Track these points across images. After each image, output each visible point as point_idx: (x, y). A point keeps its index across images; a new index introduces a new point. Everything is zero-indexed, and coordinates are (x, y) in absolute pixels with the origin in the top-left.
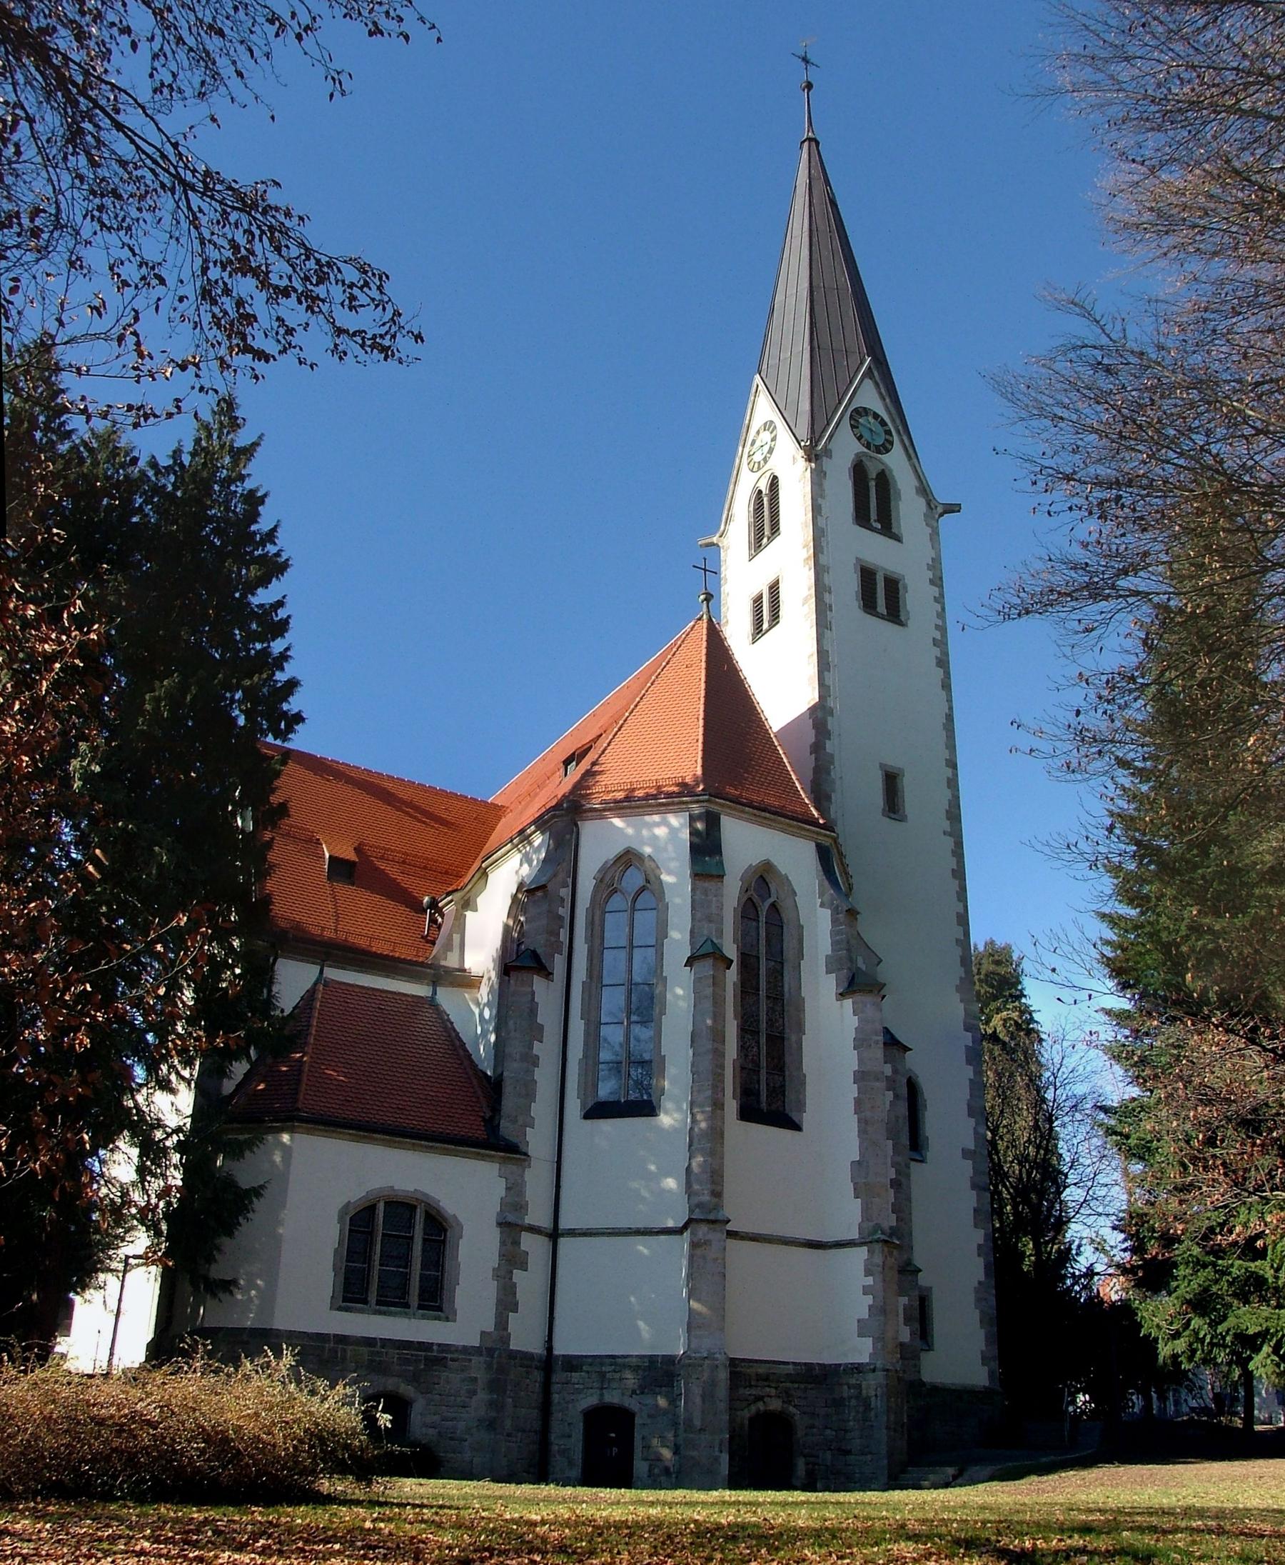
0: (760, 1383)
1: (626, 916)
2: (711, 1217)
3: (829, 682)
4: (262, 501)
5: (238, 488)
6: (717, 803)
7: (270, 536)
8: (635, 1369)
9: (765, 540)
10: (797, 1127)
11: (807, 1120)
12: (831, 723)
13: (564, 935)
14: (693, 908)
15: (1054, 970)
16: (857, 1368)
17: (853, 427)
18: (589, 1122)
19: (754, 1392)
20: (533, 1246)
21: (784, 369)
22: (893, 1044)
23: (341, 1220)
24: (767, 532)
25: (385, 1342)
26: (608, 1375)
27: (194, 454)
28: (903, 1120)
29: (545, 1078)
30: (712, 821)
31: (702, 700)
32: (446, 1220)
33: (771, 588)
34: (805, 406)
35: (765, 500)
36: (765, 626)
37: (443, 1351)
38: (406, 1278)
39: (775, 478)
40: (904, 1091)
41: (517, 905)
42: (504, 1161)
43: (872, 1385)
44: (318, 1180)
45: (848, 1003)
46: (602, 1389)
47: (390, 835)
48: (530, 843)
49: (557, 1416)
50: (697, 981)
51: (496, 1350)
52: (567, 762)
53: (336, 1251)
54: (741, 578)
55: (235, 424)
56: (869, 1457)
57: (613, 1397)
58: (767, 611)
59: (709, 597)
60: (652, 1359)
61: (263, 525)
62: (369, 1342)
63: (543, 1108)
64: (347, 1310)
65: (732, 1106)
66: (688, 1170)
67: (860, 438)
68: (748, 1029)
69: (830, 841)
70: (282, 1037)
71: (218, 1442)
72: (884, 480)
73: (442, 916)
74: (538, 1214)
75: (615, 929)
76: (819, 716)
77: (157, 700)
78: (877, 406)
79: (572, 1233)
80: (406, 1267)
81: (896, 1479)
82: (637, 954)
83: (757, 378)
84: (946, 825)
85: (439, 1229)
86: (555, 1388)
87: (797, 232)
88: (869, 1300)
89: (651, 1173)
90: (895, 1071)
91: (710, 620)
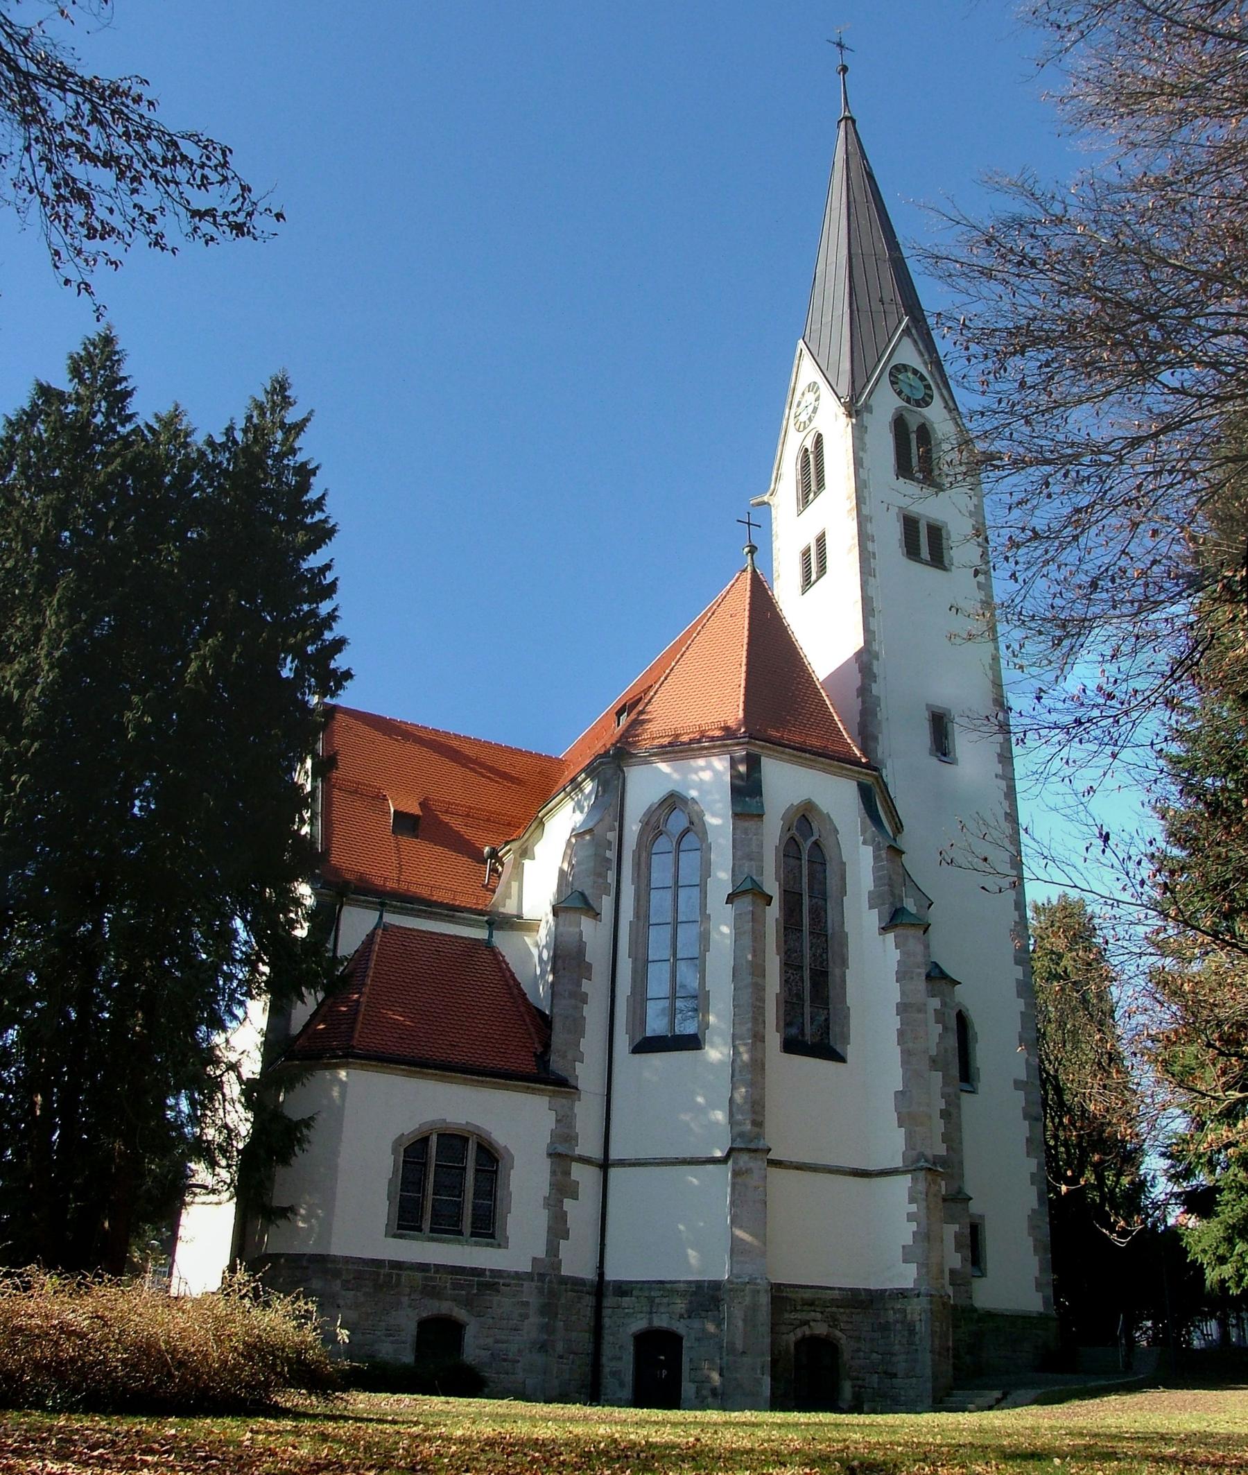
0: (806, 1308)
1: (671, 856)
2: (753, 1146)
3: (874, 625)
4: (313, 472)
5: (291, 461)
6: (755, 745)
7: (319, 504)
8: (683, 1294)
9: (812, 496)
10: (841, 1059)
11: (851, 1052)
12: (877, 667)
13: (611, 877)
14: (734, 847)
15: (985, 860)
16: (902, 1294)
17: (893, 383)
19: (798, 1316)
20: (584, 1176)
21: (826, 331)
22: (938, 977)
23: (395, 1151)
24: (813, 488)
25: (439, 1268)
26: (657, 1300)
27: (245, 431)
28: (958, 1055)
29: (594, 1014)
30: (753, 762)
31: (745, 647)
32: (497, 1150)
33: (818, 540)
34: (846, 365)
35: (811, 457)
36: (814, 577)
37: (495, 1277)
38: (459, 1206)
39: (820, 435)
40: (953, 1023)
41: (571, 848)
42: (553, 1095)
43: (917, 1309)
44: (374, 1113)
45: (890, 937)
46: (651, 1313)
47: (454, 789)
48: (582, 791)
49: (608, 1338)
50: (738, 917)
51: (548, 1279)
52: (619, 714)
53: (390, 1180)
54: (790, 532)
55: (287, 402)
56: (914, 1380)
57: (661, 1322)
58: (814, 564)
59: (753, 550)
60: (699, 1285)
61: (312, 495)
62: (423, 1267)
63: (592, 1043)
64: (401, 1237)
65: (774, 1039)
66: (731, 1100)
67: (899, 393)
68: (790, 965)
69: (871, 779)
70: (339, 982)
71: (147, 1353)
72: (924, 433)
73: (502, 865)
74: (589, 1146)
75: (661, 873)
76: (865, 661)
77: (204, 658)
78: (916, 361)
79: (622, 1163)
80: (459, 1196)
81: (941, 1402)
82: (683, 893)
83: (801, 344)
84: (999, 769)
85: (490, 1159)
86: (606, 1312)
87: (835, 204)
88: (913, 1226)
89: (699, 1104)
90: (944, 1004)
91: (754, 571)
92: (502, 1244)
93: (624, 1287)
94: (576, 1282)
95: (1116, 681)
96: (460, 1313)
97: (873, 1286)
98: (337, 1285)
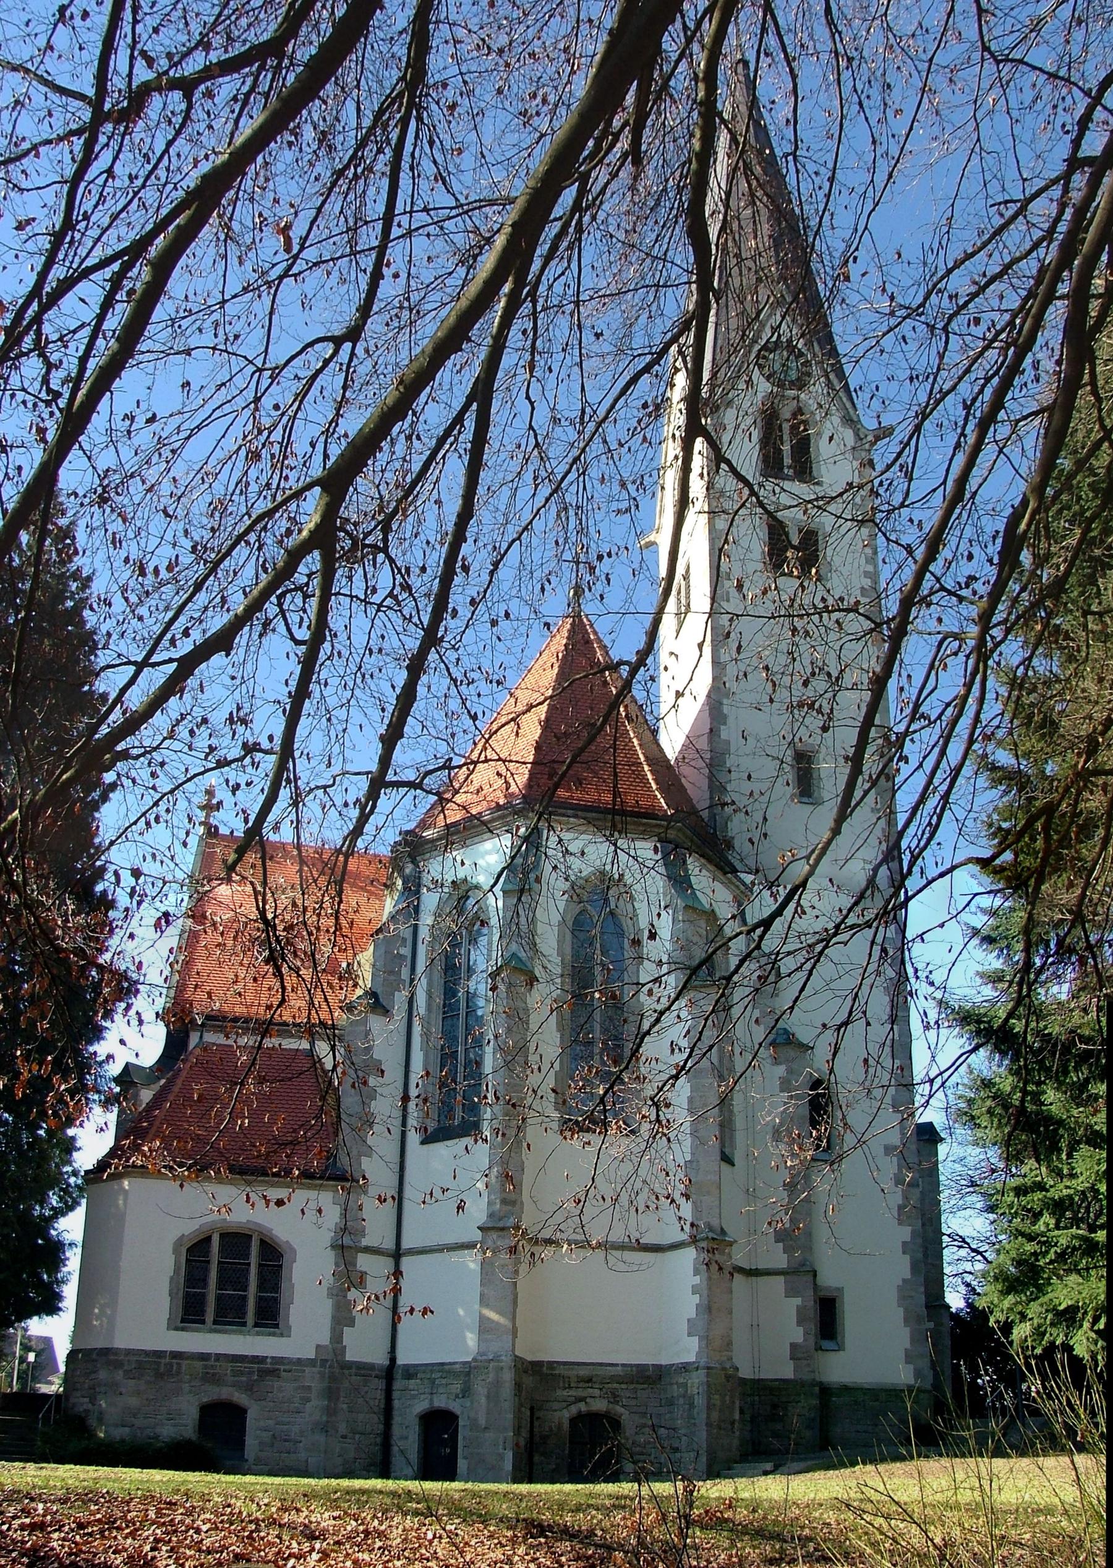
2: (501, 1225)
13: (405, 973)
16: (685, 1368)
18: (432, 1146)
19: (572, 1393)
20: (375, 1268)
23: (176, 1251)
25: (218, 1357)
38: (244, 1299)
43: (696, 1382)
49: (397, 1419)
51: (334, 1367)
53: (172, 1278)
57: (440, 1402)
62: (204, 1357)
64: (183, 1329)
79: (412, 1252)
85: (273, 1256)
88: (696, 1299)
92: (286, 1333)
93: (411, 1371)
94: (363, 1369)
95: (745, 675)
96: (240, 1398)
97: (664, 1362)
98: (119, 1375)
